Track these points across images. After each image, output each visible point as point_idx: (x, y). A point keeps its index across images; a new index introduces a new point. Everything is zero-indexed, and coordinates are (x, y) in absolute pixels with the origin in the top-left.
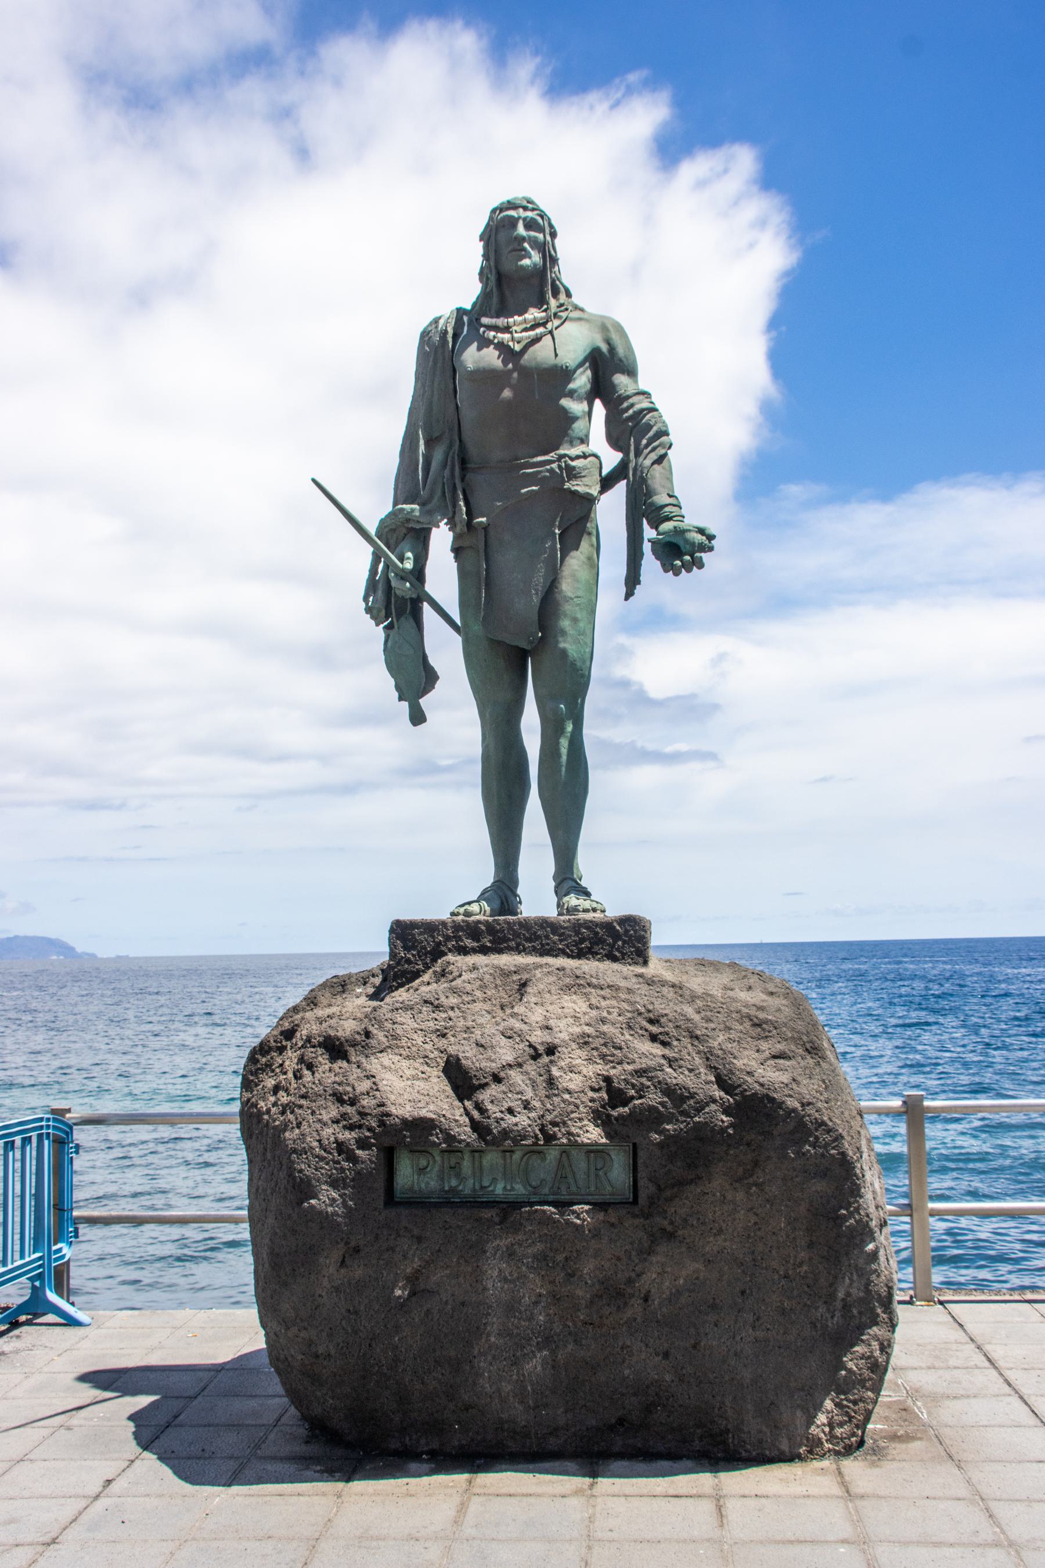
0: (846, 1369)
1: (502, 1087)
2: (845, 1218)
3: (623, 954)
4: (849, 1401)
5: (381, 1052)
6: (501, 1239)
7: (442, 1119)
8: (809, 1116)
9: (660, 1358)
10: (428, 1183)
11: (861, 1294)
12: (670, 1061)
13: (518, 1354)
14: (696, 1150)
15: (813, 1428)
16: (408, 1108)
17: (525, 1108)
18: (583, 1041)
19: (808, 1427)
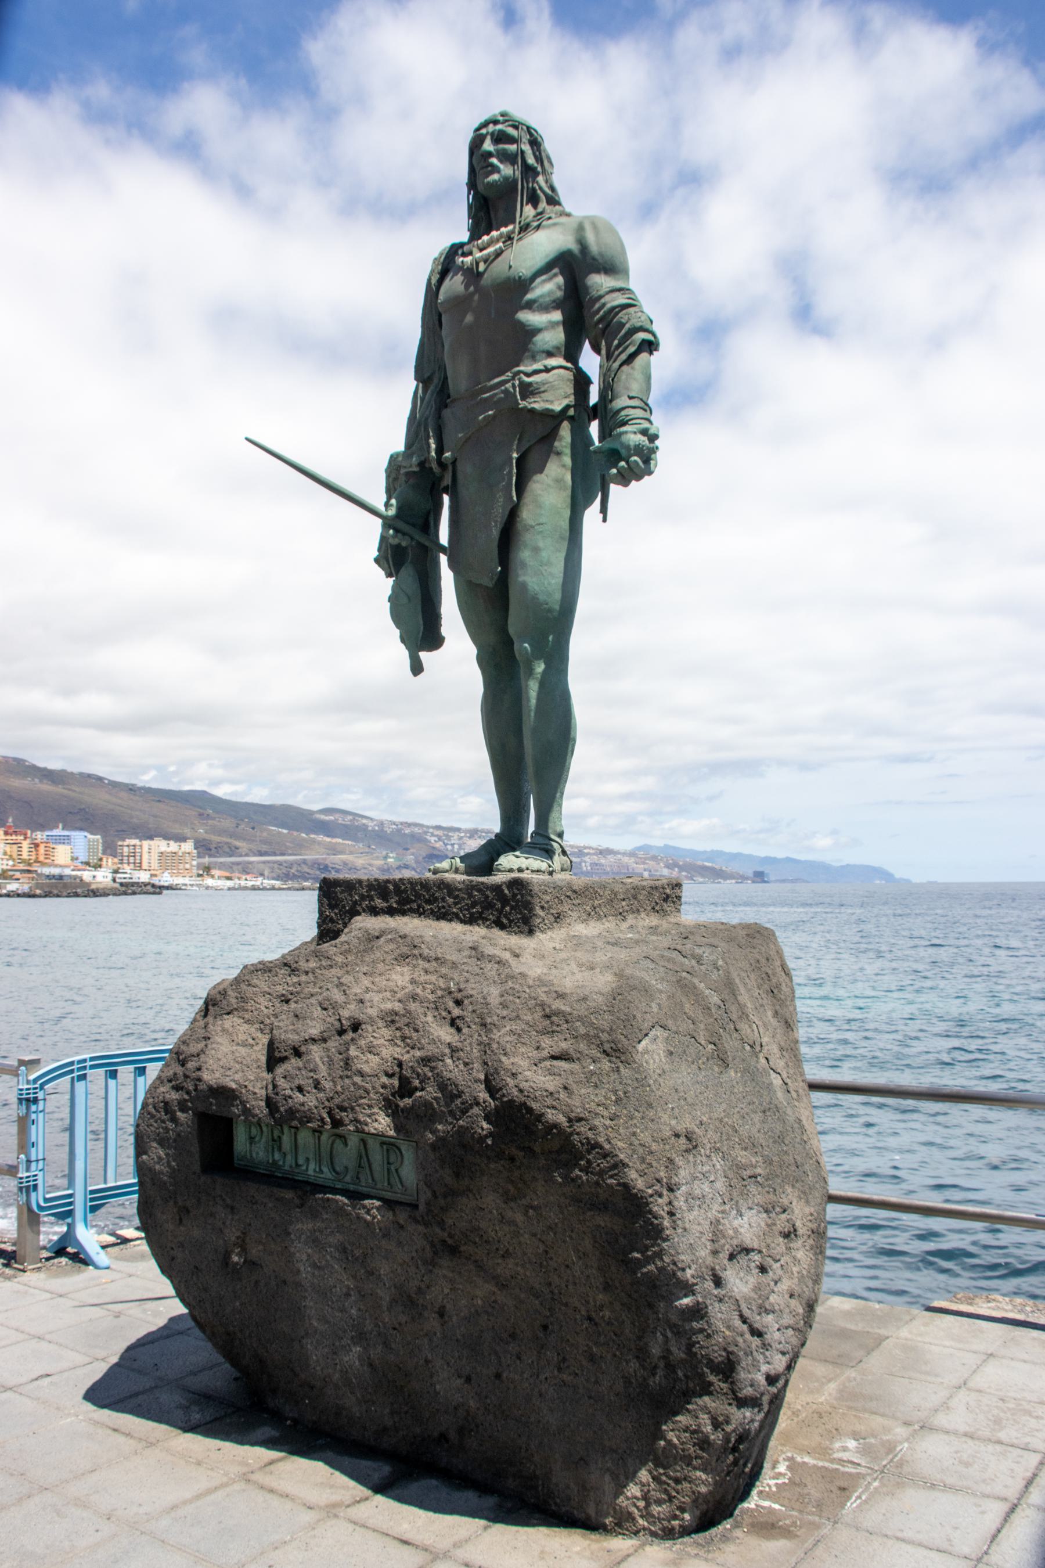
0: (665, 1440)
1: (300, 1063)
2: (639, 1264)
3: (511, 921)
4: (670, 1478)
5: (228, 1014)
6: (302, 1222)
7: (244, 1091)
8: (578, 1134)
9: (462, 1380)
10: (257, 1153)
11: (683, 1356)
12: (453, 1051)
13: (337, 1344)
14: (459, 1156)
15: (621, 1498)
16: (217, 1075)
17: (316, 1088)
18: (391, 1019)
19: (616, 1497)
